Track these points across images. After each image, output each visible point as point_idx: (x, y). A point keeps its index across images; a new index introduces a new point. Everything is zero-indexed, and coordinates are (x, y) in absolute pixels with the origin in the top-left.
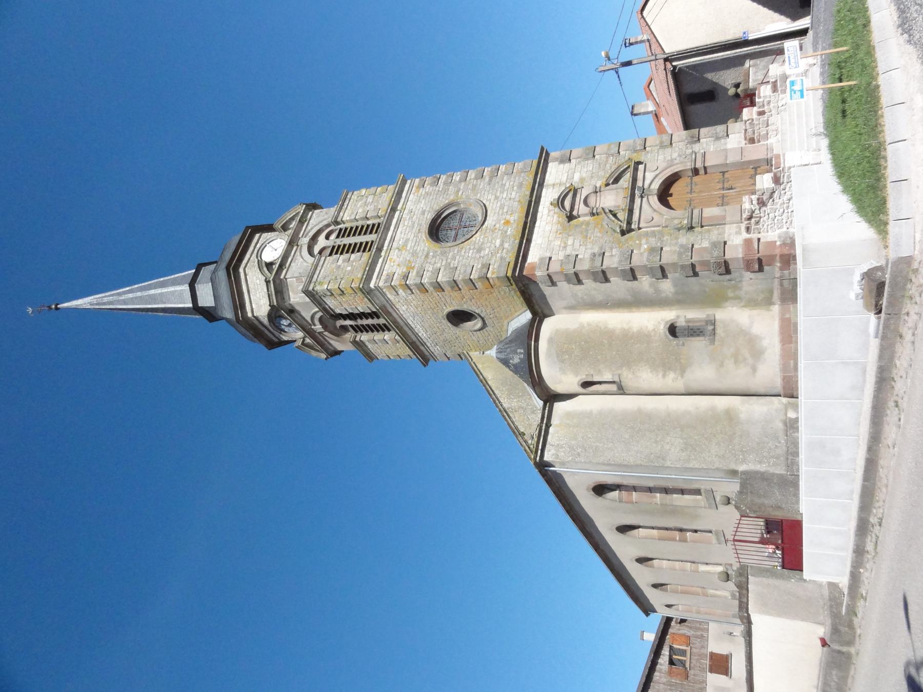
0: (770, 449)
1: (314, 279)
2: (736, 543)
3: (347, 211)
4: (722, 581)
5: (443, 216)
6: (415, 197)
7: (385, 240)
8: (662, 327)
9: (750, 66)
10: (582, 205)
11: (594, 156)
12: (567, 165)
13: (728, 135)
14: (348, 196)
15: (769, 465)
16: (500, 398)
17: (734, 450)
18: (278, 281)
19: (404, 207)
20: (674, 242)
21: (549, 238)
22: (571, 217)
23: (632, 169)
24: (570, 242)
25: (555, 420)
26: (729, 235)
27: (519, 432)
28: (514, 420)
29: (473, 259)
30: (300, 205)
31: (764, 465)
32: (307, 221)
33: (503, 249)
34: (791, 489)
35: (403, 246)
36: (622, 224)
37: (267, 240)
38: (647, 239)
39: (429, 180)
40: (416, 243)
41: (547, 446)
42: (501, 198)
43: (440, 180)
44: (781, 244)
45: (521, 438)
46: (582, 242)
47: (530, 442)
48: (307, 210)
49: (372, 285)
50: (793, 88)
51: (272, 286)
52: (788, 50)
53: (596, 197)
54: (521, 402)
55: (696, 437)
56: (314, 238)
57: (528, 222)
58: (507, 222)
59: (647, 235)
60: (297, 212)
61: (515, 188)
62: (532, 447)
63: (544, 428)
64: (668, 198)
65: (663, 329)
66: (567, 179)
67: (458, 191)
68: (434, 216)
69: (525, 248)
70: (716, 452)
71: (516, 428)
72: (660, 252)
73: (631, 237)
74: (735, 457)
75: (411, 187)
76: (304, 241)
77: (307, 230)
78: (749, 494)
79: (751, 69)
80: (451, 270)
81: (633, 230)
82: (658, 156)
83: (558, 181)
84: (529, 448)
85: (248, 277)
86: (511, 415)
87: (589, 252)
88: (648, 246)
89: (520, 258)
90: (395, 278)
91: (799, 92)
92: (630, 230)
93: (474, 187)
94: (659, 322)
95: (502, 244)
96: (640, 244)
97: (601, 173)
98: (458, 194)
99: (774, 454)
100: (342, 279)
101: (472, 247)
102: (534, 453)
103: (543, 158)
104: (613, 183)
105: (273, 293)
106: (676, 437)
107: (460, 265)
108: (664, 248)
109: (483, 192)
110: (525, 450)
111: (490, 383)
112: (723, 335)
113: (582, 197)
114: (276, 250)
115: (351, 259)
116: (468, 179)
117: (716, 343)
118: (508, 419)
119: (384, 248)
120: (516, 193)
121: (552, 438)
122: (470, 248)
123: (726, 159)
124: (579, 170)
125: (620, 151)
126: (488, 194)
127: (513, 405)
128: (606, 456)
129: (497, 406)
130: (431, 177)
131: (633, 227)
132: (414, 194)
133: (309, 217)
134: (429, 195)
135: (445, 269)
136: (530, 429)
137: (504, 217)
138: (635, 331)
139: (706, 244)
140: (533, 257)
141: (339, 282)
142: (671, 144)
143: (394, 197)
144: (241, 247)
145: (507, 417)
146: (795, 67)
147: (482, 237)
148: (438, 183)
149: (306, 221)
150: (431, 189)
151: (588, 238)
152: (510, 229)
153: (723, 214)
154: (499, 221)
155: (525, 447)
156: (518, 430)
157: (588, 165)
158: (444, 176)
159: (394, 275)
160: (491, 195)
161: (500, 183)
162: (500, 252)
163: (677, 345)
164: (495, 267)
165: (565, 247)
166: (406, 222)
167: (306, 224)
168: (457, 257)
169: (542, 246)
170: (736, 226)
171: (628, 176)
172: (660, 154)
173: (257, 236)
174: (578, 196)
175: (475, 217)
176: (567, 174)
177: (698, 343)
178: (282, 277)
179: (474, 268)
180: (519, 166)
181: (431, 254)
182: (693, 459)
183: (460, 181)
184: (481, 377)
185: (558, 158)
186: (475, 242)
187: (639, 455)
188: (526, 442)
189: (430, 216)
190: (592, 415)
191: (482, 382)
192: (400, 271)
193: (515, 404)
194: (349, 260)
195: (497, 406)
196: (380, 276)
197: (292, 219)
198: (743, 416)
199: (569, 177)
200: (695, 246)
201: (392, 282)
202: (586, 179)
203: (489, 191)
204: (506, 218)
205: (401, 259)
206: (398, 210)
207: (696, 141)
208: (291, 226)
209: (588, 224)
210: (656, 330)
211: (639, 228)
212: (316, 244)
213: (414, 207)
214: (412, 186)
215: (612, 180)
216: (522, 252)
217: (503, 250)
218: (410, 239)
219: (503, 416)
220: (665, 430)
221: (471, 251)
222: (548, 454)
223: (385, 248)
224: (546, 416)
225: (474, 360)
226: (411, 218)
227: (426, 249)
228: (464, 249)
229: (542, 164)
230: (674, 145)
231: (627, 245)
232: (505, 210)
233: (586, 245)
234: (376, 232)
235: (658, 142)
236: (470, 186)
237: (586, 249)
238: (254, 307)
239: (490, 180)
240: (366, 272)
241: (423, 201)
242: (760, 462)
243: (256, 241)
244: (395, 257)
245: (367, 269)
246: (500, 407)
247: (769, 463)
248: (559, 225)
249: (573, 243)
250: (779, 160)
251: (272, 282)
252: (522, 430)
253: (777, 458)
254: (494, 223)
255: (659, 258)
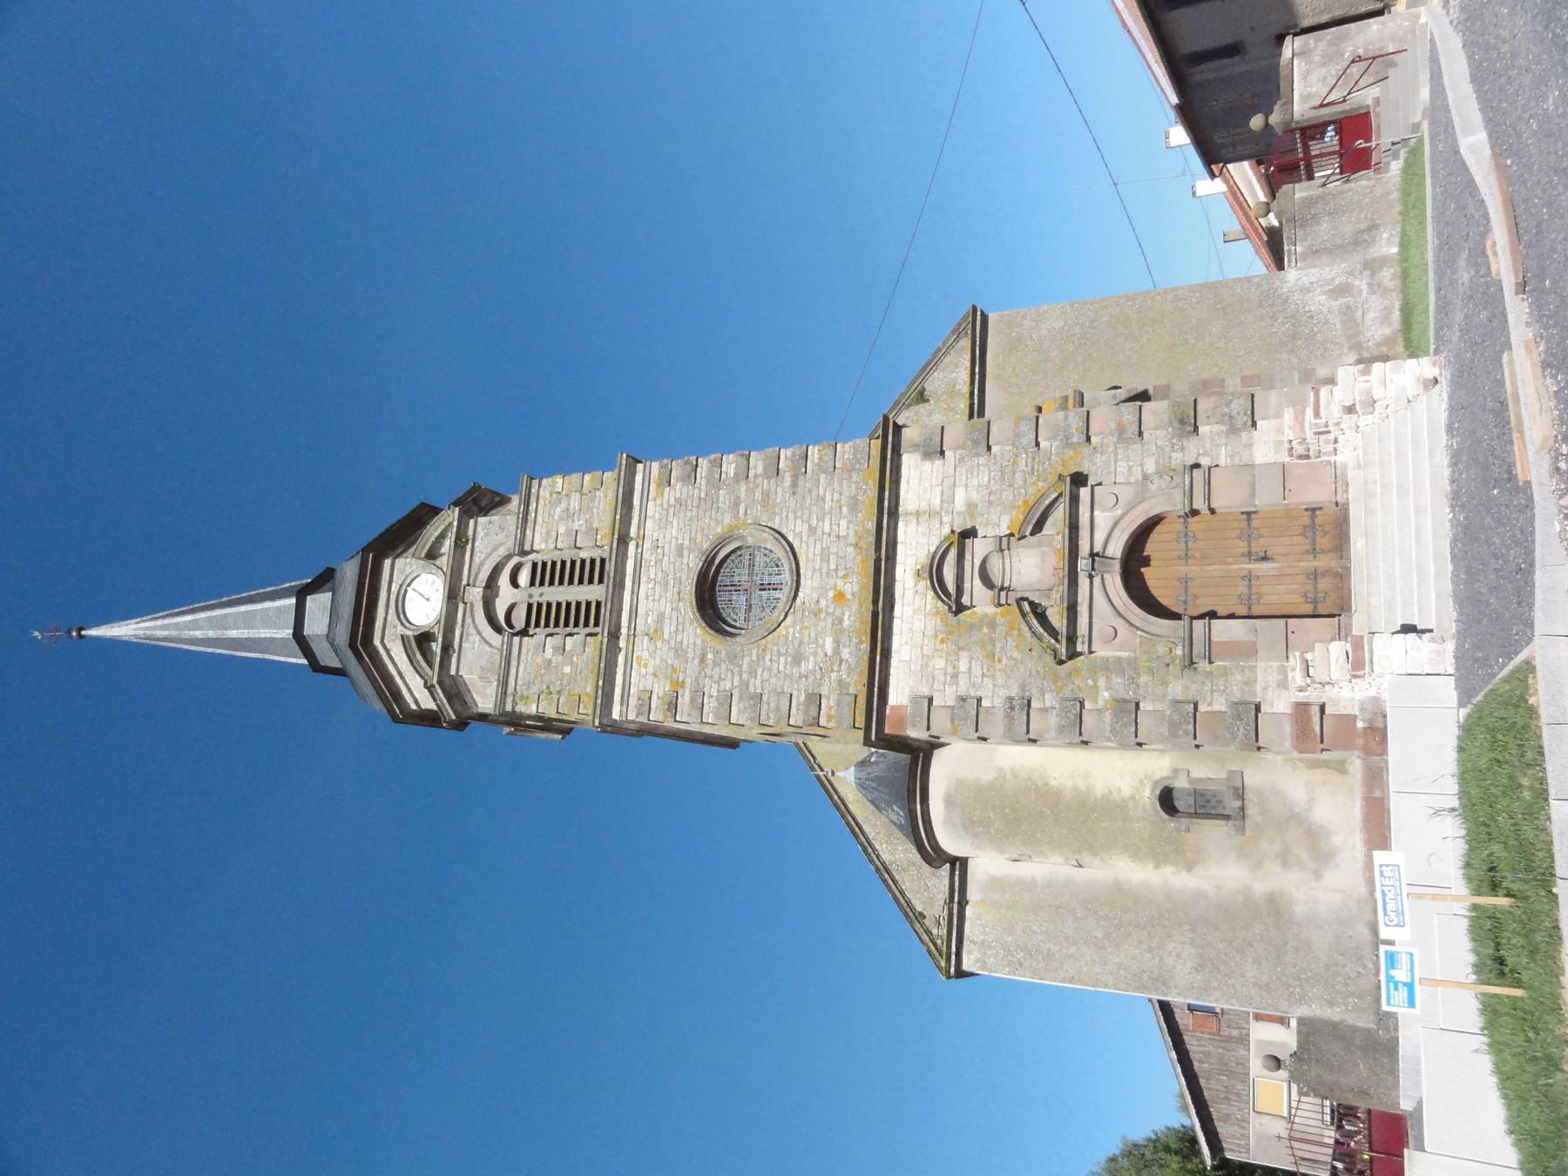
0: (1349, 978)
1: (510, 690)
2: (1295, 1144)
3: (537, 527)
4: (1272, 1071)
5: (717, 561)
6: (658, 509)
7: (620, 610)
8: (1147, 792)
9: (1293, 56)
10: (977, 582)
11: (989, 448)
12: (938, 463)
13: (1254, 424)
14: (533, 490)
15: (1347, 1010)
16: (873, 842)
17: (1285, 975)
18: (447, 681)
19: (642, 533)
20: (1159, 692)
21: (922, 649)
22: (960, 609)
23: (1066, 499)
24: (963, 666)
25: (973, 894)
26: (1265, 688)
27: (914, 914)
28: (904, 888)
29: (788, 679)
30: (449, 509)
31: (1338, 1010)
32: (470, 542)
33: (841, 661)
34: (1385, 1061)
35: (656, 630)
36: (1058, 646)
37: (407, 576)
38: (1107, 678)
39: (677, 468)
40: (677, 624)
41: (965, 943)
42: (819, 532)
43: (699, 469)
44: (1365, 729)
45: (919, 925)
46: (985, 667)
47: (935, 931)
48: (465, 517)
49: (616, 715)
50: (1392, 972)
51: (440, 691)
52: (1382, 875)
53: (1003, 557)
54: (911, 852)
55: (1220, 946)
56: (491, 585)
57: (880, 610)
58: (840, 596)
59: (1107, 669)
60: (447, 523)
61: (845, 509)
62: (939, 942)
63: (955, 911)
64: (1142, 570)
65: (1148, 797)
66: (942, 501)
67: (737, 505)
68: (700, 565)
69: (880, 670)
70: (1254, 976)
71: (908, 903)
72: (1134, 715)
73: (1077, 671)
74: (1288, 989)
75: (646, 484)
76: (475, 594)
77: (474, 571)
78: (1313, 1063)
79: (1296, 62)
80: (752, 702)
81: (1080, 654)
82: (1116, 462)
83: (924, 506)
84: (935, 944)
85: (391, 653)
86: (897, 877)
87: (1002, 693)
88: (1111, 695)
89: (875, 699)
90: (653, 706)
91: (1405, 988)
92: (1073, 655)
93: (766, 494)
94: (1141, 782)
95: (837, 651)
96: (1096, 687)
97: (1007, 495)
98: (738, 512)
99: (1354, 989)
100: (559, 692)
101: (783, 651)
102: (944, 957)
103: (890, 446)
104: (1033, 533)
105: (445, 701)
106: (1184, 943)
107: (766, 691)
108: (1141, 705)
109: (785, 514)
110: (929, 952)
111: (852, 808)
112: (1259, 819)
113: (975, 560)
114: (428, 600)
115: (568, 648)
116: (751, 474)
117: (1247, 833)
118: (893, 887)
119: (622, 631)
120: (849, 522)
121: (972, 926)
122: (779, 652)
123: (1253, 495)
124: (964, 482)
125: (1039, 440)
126: (795, 519)
127: (897, 857)
128: (1067, 971)
129: (871, 861)
130: (679, 461)
131: (1079, 648)
132: (654, 499)
133: (470, 533)
134: (683, 507)
135: (741, 698)
136: (932, 907)
137: (832, 582)
138: (1099, 797)
139: (1221, 704)
140: (899, 693)
141: (556, 701)
142: (1140, 434)
143: (619, 512)
144: (362, 624)
145: (891, 882)
146: (1397, 926)
147: (798, 628)
148: (695, 478)
149: (467, 542)
150: (685, 491)
151: (996, 659)
152: (847, 614)
153: (1251, 638)
154: (823, 590)
155: (928, 946)
156: (912, 908)
157: (979, 468)
158: (705, 462)
159: (650, 698)
160: (800, 520)
161: (814, 493)
162: (835, 668)
163: (1177, 829)
164: (832, 703)
165: (955, 676)
166: (651, 573)
167: (469, 547)
168: (759, 672)
169: (913, 667)
170: (1278, 667)
171: (1060, 514)
172: (1119, 457)
173: (387, 562)
174: (968, 556)
175: (777, 566)
176: (940, 488)
177: (1214, 830)
178: (453, 672)
179: (794, 701)
180: (845, 450)
181: (710, 656)
182: (1215, 988)
183: (737, 478)
184: (835, 797)
185: (918, 445)
186: (786, 636)
187: (1122, 972)
188: (928, 932)
189: (694, 563)
190: (1036, 886)
191: (838, 809)
192: (661, 689)
193: (902, 855)
194: (564, 651)
195: (871, 861)
196: (626, 698)
197: (442, 536)
198: (1299, 910)
199: (945, 498)
200: (1202, 708)
201: (649, 713)
202: (980, 505)
203: (795, 512)
204: (836, 586)
205: (658, 659)
206: (632, 539)
207: (1189, 432)
208: (443, 550)
209: (993, 625)
210: (1137, 797)
211: (1091, 652)
212: (497, 596)
213: (661, 535)
214: (647, 481)
215: (1030, 528)
216: (876, 684)
217: (840, 665)
218: (666, 616)
219: (884, 881)
220: (1165, 927)
221: (782, 659)
222: (969, 959)
223: (624, 631)
224: (957, 888)
225: (819, 759)
226: (659, 561)
227: (699, 642)
228: (768, 652)
229: (888, 463)
230: (1146, 435)
231: (1071, 687)
232: (832, 566)
233: (993, 676)
234: (601, 581)
235: (1113, 425)
236: (758, 496)
237: (995, 686)
238: (417, 696)
239: (794, 484)
240: (600, 692)
241: (675, 523)
242: (1331, 1003)
243: (388, 579)
244: (645, 655)
245: (600, 683)
246: (877, 862)
247: (1346, 1004)
248: (938, 618)
249: (970, 668)
250: (1360, 653)
251: (437, 686)
252: (919, 908)
253: (1361, 997)
254: (815, 595)
255: (1133, 730)
